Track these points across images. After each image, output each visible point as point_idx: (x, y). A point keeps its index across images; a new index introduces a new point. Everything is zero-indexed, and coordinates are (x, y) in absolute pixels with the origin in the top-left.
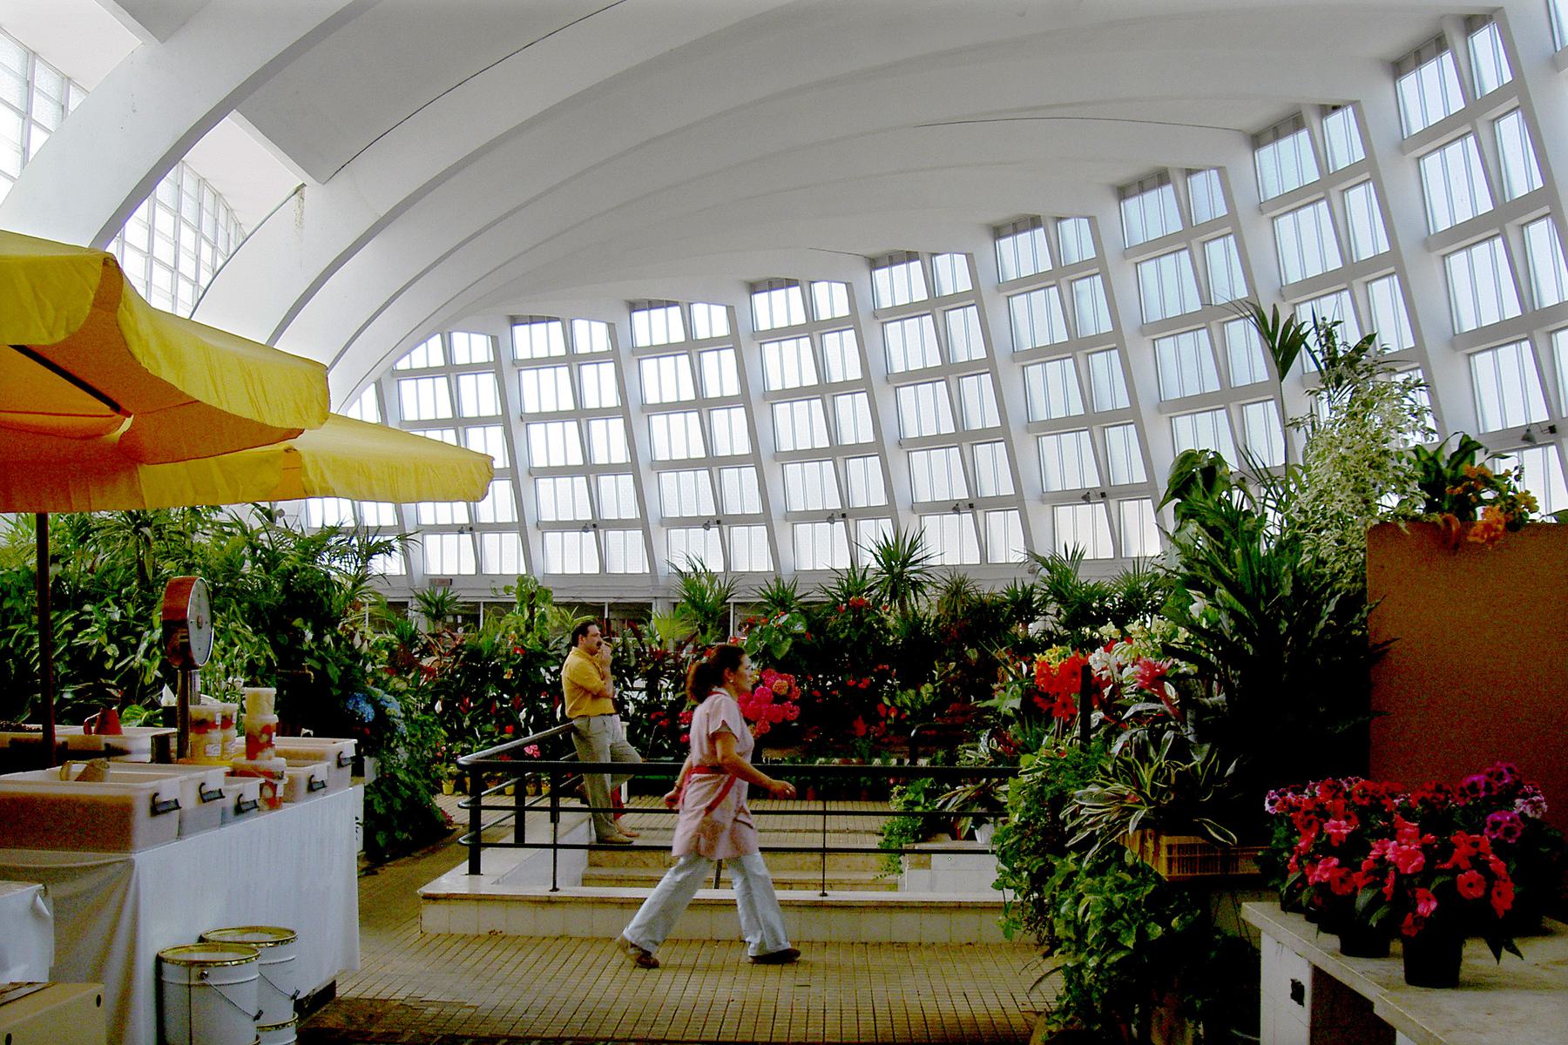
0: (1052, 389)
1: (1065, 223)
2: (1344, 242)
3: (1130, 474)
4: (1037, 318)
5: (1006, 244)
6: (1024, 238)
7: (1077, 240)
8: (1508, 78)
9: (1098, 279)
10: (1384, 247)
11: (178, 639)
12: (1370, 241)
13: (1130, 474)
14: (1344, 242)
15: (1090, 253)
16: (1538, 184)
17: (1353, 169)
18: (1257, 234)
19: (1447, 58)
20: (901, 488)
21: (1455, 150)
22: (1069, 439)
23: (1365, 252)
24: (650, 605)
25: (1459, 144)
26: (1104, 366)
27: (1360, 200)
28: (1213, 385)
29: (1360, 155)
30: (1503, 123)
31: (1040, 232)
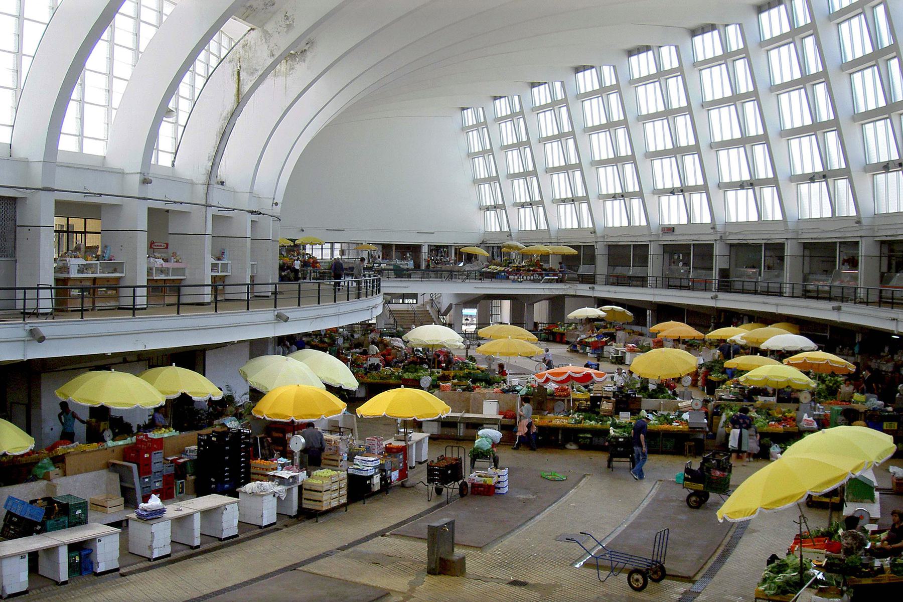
0: (724, 124)
1: (729, 27)
2: (733, 85)
3: (766, 173)
4: (715, 83)
5: (698, 39)
6: (707, 36)
7: (669, 57)
8: (809, 21)
9: (680, 78)
10: (751, 89)
11: (553, 264)
12: (678, 100)
13: (766, 173)
14: (733, 85)
15: (676, 64)
16: (821, 69)
17: (738, 52)
18: (628, 94)
19: (782, 7)
20: (856, 153)
21: (784, 49)
22: (733, 152)
23: (743, 90)
24: (857, 243)
25: (786, 47)
26: (682, 122)
27: (614, 98)
28: (737, 135)
29: (741, 46)
30: (807, 39)
31: (716, 33)
